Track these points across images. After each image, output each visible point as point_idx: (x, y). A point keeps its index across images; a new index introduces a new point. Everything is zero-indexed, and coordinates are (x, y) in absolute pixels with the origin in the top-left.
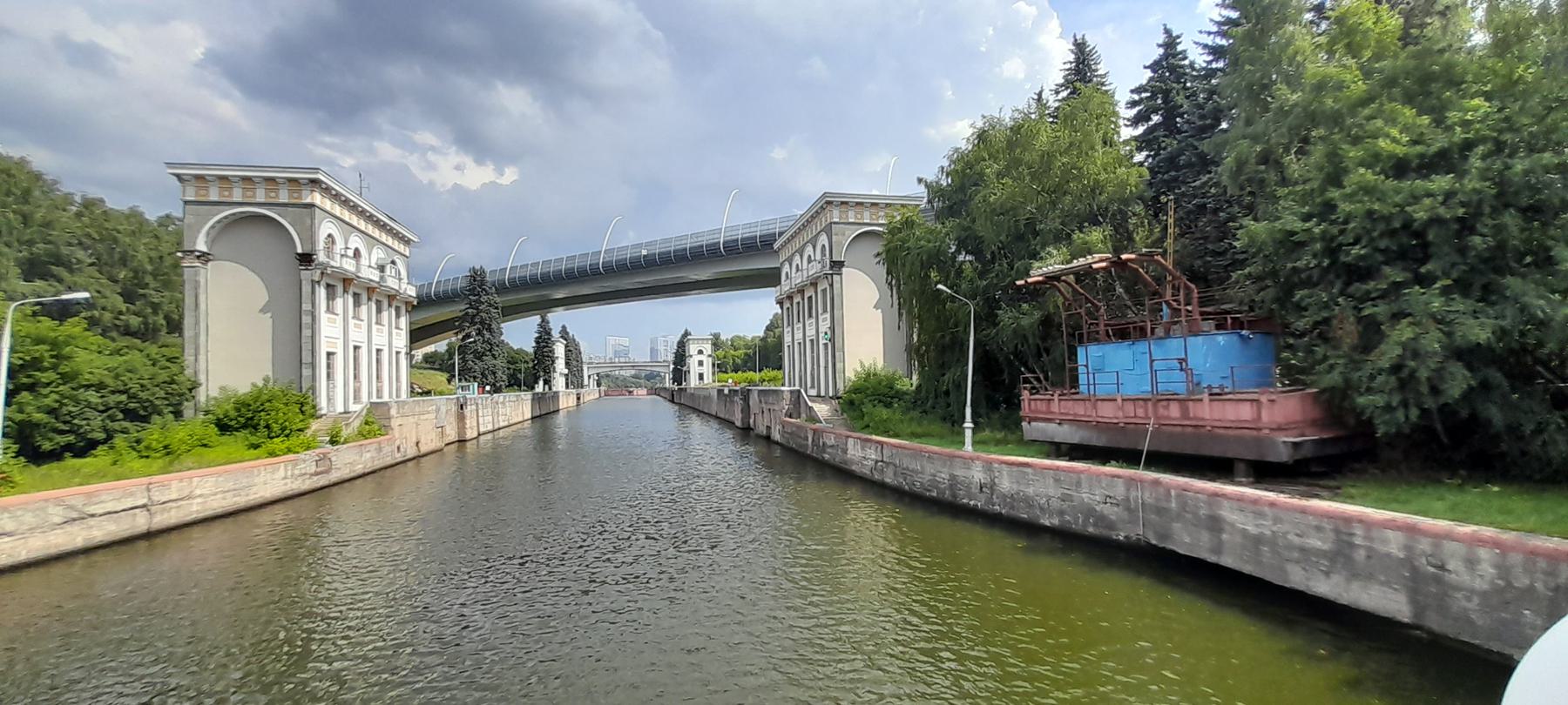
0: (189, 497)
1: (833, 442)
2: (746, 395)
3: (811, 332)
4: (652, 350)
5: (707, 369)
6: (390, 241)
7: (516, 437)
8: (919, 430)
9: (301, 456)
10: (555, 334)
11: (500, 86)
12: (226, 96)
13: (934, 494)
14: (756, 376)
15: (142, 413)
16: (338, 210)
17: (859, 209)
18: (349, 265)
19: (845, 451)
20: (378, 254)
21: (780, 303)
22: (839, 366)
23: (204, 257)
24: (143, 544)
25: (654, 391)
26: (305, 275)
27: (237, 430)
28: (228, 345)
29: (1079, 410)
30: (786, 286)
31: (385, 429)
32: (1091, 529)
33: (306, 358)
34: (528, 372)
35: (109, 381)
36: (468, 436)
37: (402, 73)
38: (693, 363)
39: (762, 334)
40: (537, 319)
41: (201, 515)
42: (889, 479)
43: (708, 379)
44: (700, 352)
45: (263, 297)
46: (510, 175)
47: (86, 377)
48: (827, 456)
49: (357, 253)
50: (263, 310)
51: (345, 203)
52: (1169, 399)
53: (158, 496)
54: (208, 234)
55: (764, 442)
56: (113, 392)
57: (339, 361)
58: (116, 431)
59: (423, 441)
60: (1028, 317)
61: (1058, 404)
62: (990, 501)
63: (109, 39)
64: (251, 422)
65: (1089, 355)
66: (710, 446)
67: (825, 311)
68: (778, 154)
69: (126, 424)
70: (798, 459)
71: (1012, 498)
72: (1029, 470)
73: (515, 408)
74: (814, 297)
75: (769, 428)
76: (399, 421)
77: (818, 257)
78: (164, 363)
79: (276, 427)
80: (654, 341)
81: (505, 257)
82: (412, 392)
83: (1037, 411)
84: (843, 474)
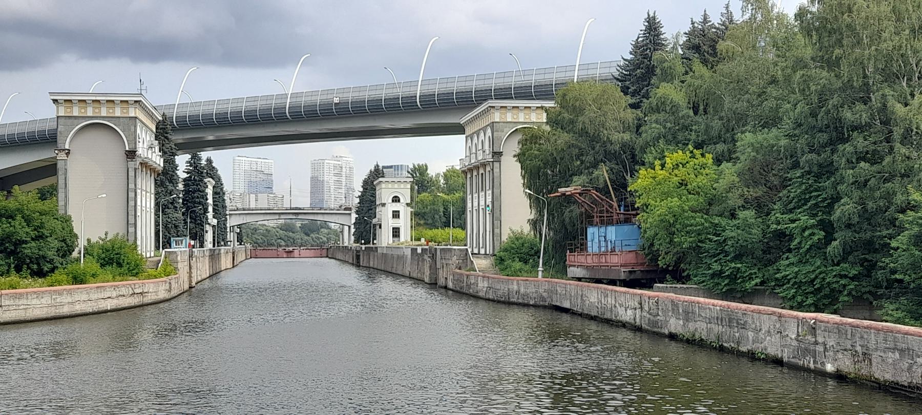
5: (404, 223)
17: (515, 111)
22: (497, 231)
26: (131, 164)
33: (132, 221)
38: (384, 216)
43: (406, 235)
44: (396, 199)
61: (581, 259)
65: (592, 232)
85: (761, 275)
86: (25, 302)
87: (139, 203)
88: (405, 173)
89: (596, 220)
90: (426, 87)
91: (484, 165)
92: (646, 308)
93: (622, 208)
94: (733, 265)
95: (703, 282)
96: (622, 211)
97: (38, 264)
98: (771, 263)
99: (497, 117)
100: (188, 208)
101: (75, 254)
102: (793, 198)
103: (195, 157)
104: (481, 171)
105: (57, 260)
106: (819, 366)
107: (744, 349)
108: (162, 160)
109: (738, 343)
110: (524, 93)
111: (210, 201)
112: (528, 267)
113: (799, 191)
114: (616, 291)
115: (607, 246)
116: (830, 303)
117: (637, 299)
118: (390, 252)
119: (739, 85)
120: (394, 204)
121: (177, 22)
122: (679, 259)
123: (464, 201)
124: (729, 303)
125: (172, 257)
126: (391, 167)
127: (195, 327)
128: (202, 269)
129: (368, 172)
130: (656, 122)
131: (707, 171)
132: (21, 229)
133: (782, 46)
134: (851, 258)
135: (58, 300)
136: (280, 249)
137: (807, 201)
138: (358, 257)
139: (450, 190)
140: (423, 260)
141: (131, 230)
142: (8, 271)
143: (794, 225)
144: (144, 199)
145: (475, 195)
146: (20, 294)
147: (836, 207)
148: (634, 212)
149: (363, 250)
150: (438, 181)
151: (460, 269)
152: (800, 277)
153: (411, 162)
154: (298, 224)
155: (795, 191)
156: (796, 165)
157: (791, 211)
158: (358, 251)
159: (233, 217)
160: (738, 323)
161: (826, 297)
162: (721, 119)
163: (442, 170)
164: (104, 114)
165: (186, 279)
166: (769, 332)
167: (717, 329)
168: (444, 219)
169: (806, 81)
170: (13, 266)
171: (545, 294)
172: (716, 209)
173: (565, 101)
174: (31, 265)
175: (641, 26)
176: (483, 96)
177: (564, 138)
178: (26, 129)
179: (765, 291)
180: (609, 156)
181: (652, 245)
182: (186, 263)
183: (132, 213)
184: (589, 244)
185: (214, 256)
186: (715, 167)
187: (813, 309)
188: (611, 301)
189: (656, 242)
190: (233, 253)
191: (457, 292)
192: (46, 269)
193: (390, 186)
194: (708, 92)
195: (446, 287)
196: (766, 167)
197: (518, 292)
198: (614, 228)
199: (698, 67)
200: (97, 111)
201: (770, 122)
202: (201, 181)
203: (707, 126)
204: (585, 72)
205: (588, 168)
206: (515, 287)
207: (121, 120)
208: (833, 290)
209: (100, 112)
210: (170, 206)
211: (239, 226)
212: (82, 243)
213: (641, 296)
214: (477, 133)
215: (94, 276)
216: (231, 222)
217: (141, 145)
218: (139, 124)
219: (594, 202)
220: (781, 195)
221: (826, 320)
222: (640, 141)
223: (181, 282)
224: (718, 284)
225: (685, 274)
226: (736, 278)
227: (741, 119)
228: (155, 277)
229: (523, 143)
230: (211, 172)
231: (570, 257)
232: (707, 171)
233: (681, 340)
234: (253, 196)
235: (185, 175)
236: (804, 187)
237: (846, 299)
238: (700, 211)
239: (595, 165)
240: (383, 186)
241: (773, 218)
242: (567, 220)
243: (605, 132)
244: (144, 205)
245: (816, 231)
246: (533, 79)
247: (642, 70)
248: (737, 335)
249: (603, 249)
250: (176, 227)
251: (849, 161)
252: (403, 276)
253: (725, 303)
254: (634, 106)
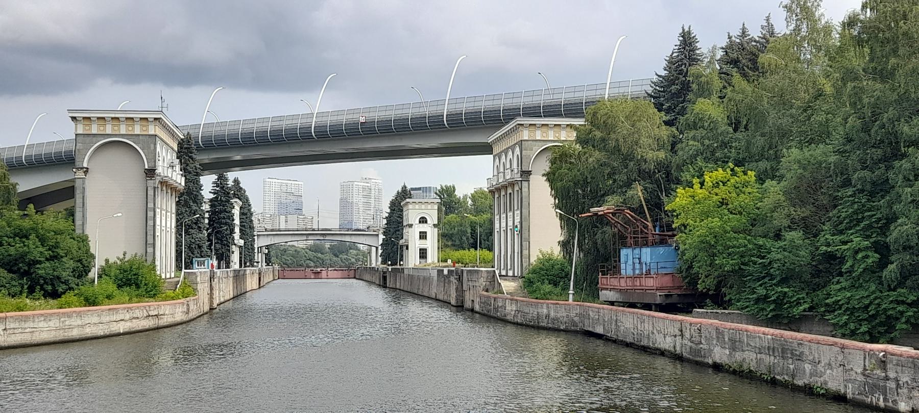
5: (432, 244)
22: (525, 252)
26: (151, 183)
33: (150, 241)
38: (412, 237)
43: (433, 256)
44: (423, 220)
61: (614, 282)
85: (809, 300)
86: (32, 325)
87: (158, 222)
88: (433, 195)
89: (630, 241)
90: (453, 106)
91: (512, 184)
92: (687, 335)
93: (657, 229)
94: (779, 289)
95: (747, 307)
96: (657, 232)
97: (53, 285)
98: (817, 288)
99: (525, 135)
100: (211, 230)
101: (91, 275)
102: (845, 218)
103: (222, 179)
104: (510, 190)
105: (73, 281)
106: (890, 404)
107: (800, 383)
108: (183, 179)
109: (793, 376)
110: (552, 111)
111: (237, 221)
112: (558, 290)
113: (851, 210)
114: (653, 317)
115: (642, 269)
116: (886, 332)
117: (678, 325)
118: (416, 274)
119: (782, 101)
120: (421, 225)
121: (208, 47)
122: (720, 282)
123: (492, 222)
124: (782, 332)
125: (192, 277)
126: (419, 189)
127: (224, 349)
128: (225, 290)
129: (395, 193)
130: (694, 138)
131: (749, 190)
132: (36, 250)
133: (835, 55)
134: (909, 283)
135: (67, 323)
136: (308, 270)
137: (859, 221)
138: (385, 278)
139: (478, 211)
140: (450, 282)
141: (150, 250)
142: (21, 293)
143: (846, 247)
144: (164, 218)
145: (503, 216)
146: (26, 316)
147: (892, 228)
148: (670, 233)
149: (391, 276)
150: (465, 202)
151: (487, 291)
152: (854, 303)
153: (437, 184)
154: (327, 245)
155: (845, 212)
156: (847, 183)
157: (841, 232)
158: (384, 273)
159: (261, 238)
160: (792, 354)
161: (881, 324)
162: (763, 135)
163: (470, 191)
164: (123, 132)
165: (206, 301)
166: (830, 364)
167: (769, 360)
168: (472, 241)
169: (858, 93)
170: (26, 287)
171: (576, 319)
172: (759, 229)
173: (596, 121)
174: (45, 286)
175: (676, 41)
176: (510, 114)
177: (597, 155)
178: (53, 150)
179: (813, 317)
180: (644, 175)
181: (691, 267)
182: (206, 285)
183: (150, 233)
184: (623, 266)
185: (239, 277)
186: (757, 185)
187: (868, 338)
188: (648, 327)
189: (696, 265)
190: (260, 274)
191: (484, 315)
192: (61, 290)
193: (417, 207)
194: (751, 108)
195: (472, 310)
196: (815, 186)
197: (548, 316)
198: (649, 250)
199: (737, 78)
200: (116, 128)
201: (822, 135)
202: (228, 201)
203: (749, 143)
204: (616, 90)
205: (621, 187)
206: (545, 311)
207: (141, 137)
208: (889, 317)
209: (119, 129)
210: (194, 226)
211: (267, 247)
212: (99, 263)
213: (681, 322)
214: (506, 152)
215: (109, 297)
216: (259, 243)
217: (160, 163)
218: (159, 142)
219: (628, 222)
220: (831, 214)
221: (899, 353)
222: (676, 160)
223: (201, 302)
224: (763, 309)
225: (727, 298)
226: (782, 304)
227: (784, 134)
228: (173, 299)
229: (553, 162)
230: (239, 192)
231: (603, 280)
232: (749, 190)
233: (727, 371)
234: (283, 218)
235: (212, 196)
236: (856, 206)
237: (904, 326)
238: (744, 231)
239: (628, 184)
240: (410, 206)
241: (822, 239)
242: (599, 241)
243: (639, 150)
244: (163, 224)
245: (870, 254)
246: (563, 98)
247: (677, 87)
248: (792, 367)
249: (637, 272)
250: (200, 247)
251: (907, 179)
252: (429, 298)
253: (777, 332)
254: (668, 123)
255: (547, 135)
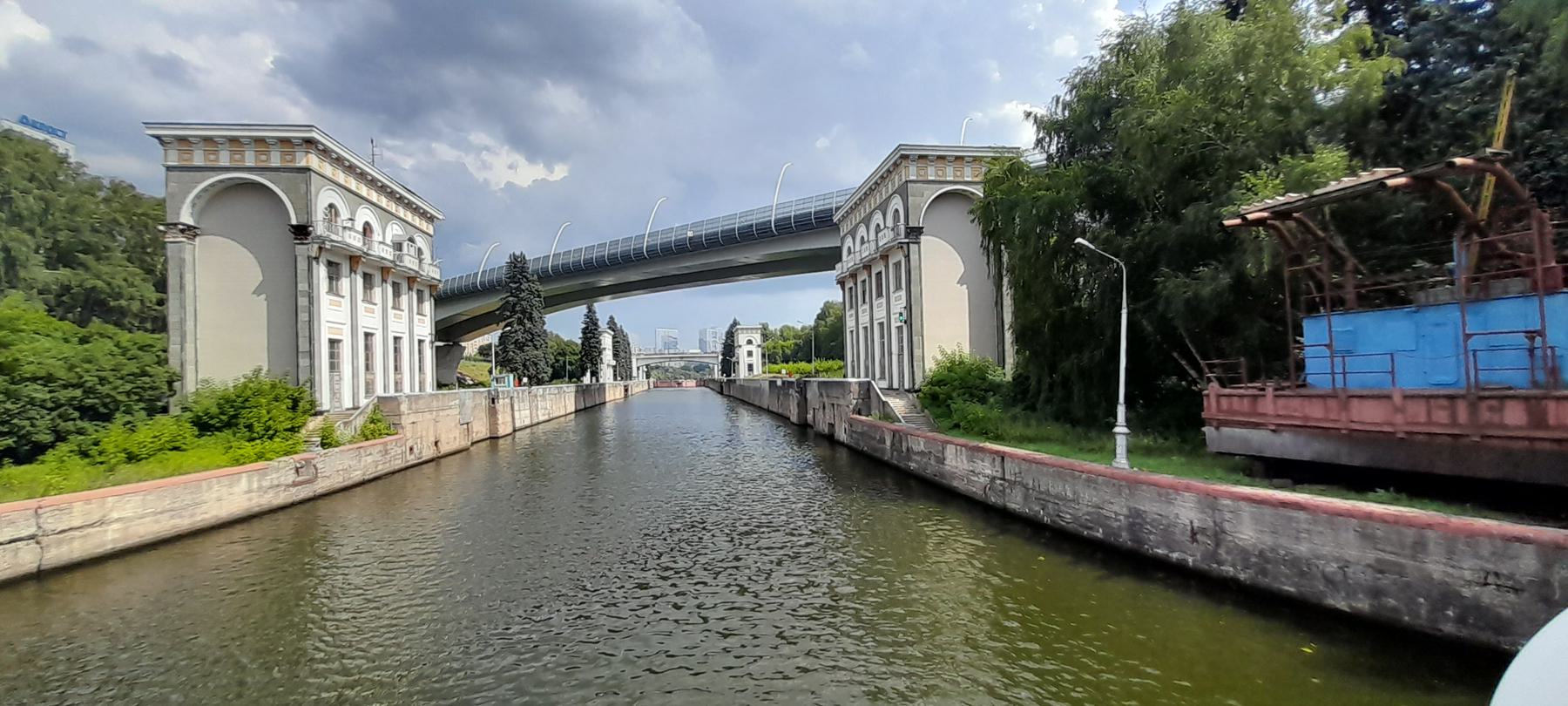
0: (101, 522)
1: (922, 447)
2: (802, 387)
3: (880, 314)
4: (701, 341)
5: (756, 360)
6: (409, 217)
7: (557, 433)
8: (1029, 432)
9: (274, 463)
10: (603, 324)
11: (549, 83)
12: (296, 103)
13: (1099, 534)
14: (810, 367)
15: (102, 410)
16: (341, 177)
18: (355, 241)
19: (941, 461)
20: (364, 215)
21: (842, 283)
22: (917, 352)
23: (190, 231)
24: (29, 590)
25: (703, 383)
26: (301, 250)
27: (219, 429)
28: (217, 330)
29: (1298, 408)
30: (847, 263)
31: (394, 427)
32: (1449, 628)
33: (303, 345)
34: (576, 365)
35: (62, 373)
36: (501, 432)
37: (455, 76)
38: (742, 354)
39: (812, 323)
40: (583, 309)
41: (120, 545)
42: (1015, 502)
43: (758, 369)
44: (750, 342)
45: (258, 277)
46: (560, 172)
47: (28, 370)
48: (913, 465)
49: (367, 230)
50: (257, 292)
51: (350, 169)
52: (1503, 397)
53: (50, 523)
54: (194, 205)
55: (826, 444)
56: (65, 387)
57: (345, 351)
58: (69, 433)
59: (443, 439)
60: (1212, 281)
62: (1213, 556)
63: (190, 53)
64: (228, 421)
65: (1314, 332)
66: (763, 449)
67: (898, 288)
68: (823, 143)
69: (85, 424)
70: (868, 468)
71: (1264, 559)
72: (1302, 515)
73: (558, 401)
74: (893, 265)
75: (832, 426)
76: (412, 418)
77: (890, 223)
78: (134, 351)
79: (258, 428)
80: (703, 332)
81: (542, 246)
82: (440, 386)
83: (1235, 413)
84: (942, 493)
200: (263, 157)
255: (944, 174)
